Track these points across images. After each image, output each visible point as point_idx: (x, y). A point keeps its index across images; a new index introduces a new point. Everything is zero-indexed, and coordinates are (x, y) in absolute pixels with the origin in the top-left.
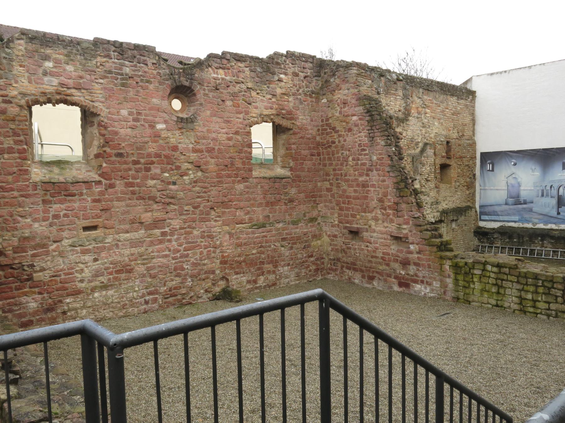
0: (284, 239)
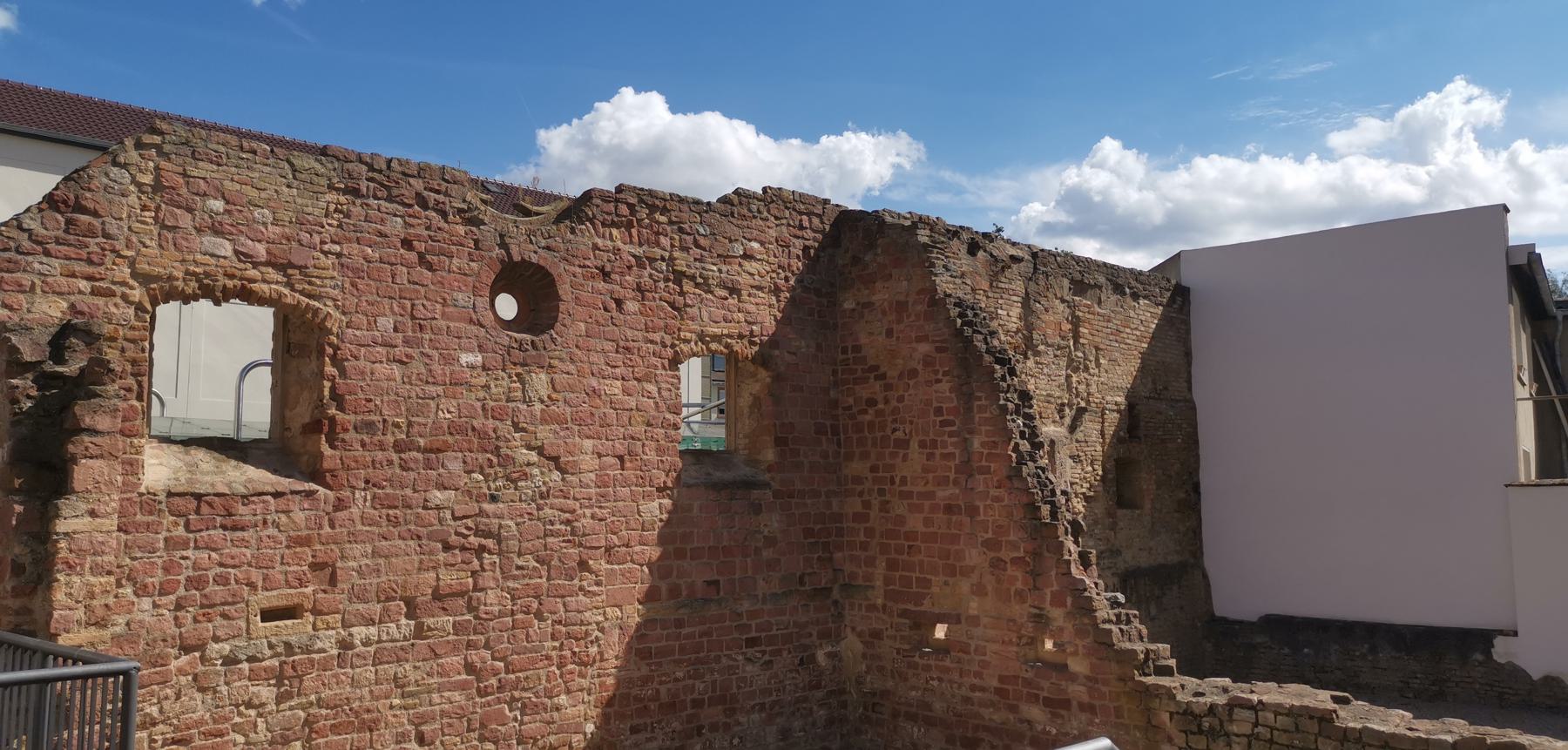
0: (752, 642)
